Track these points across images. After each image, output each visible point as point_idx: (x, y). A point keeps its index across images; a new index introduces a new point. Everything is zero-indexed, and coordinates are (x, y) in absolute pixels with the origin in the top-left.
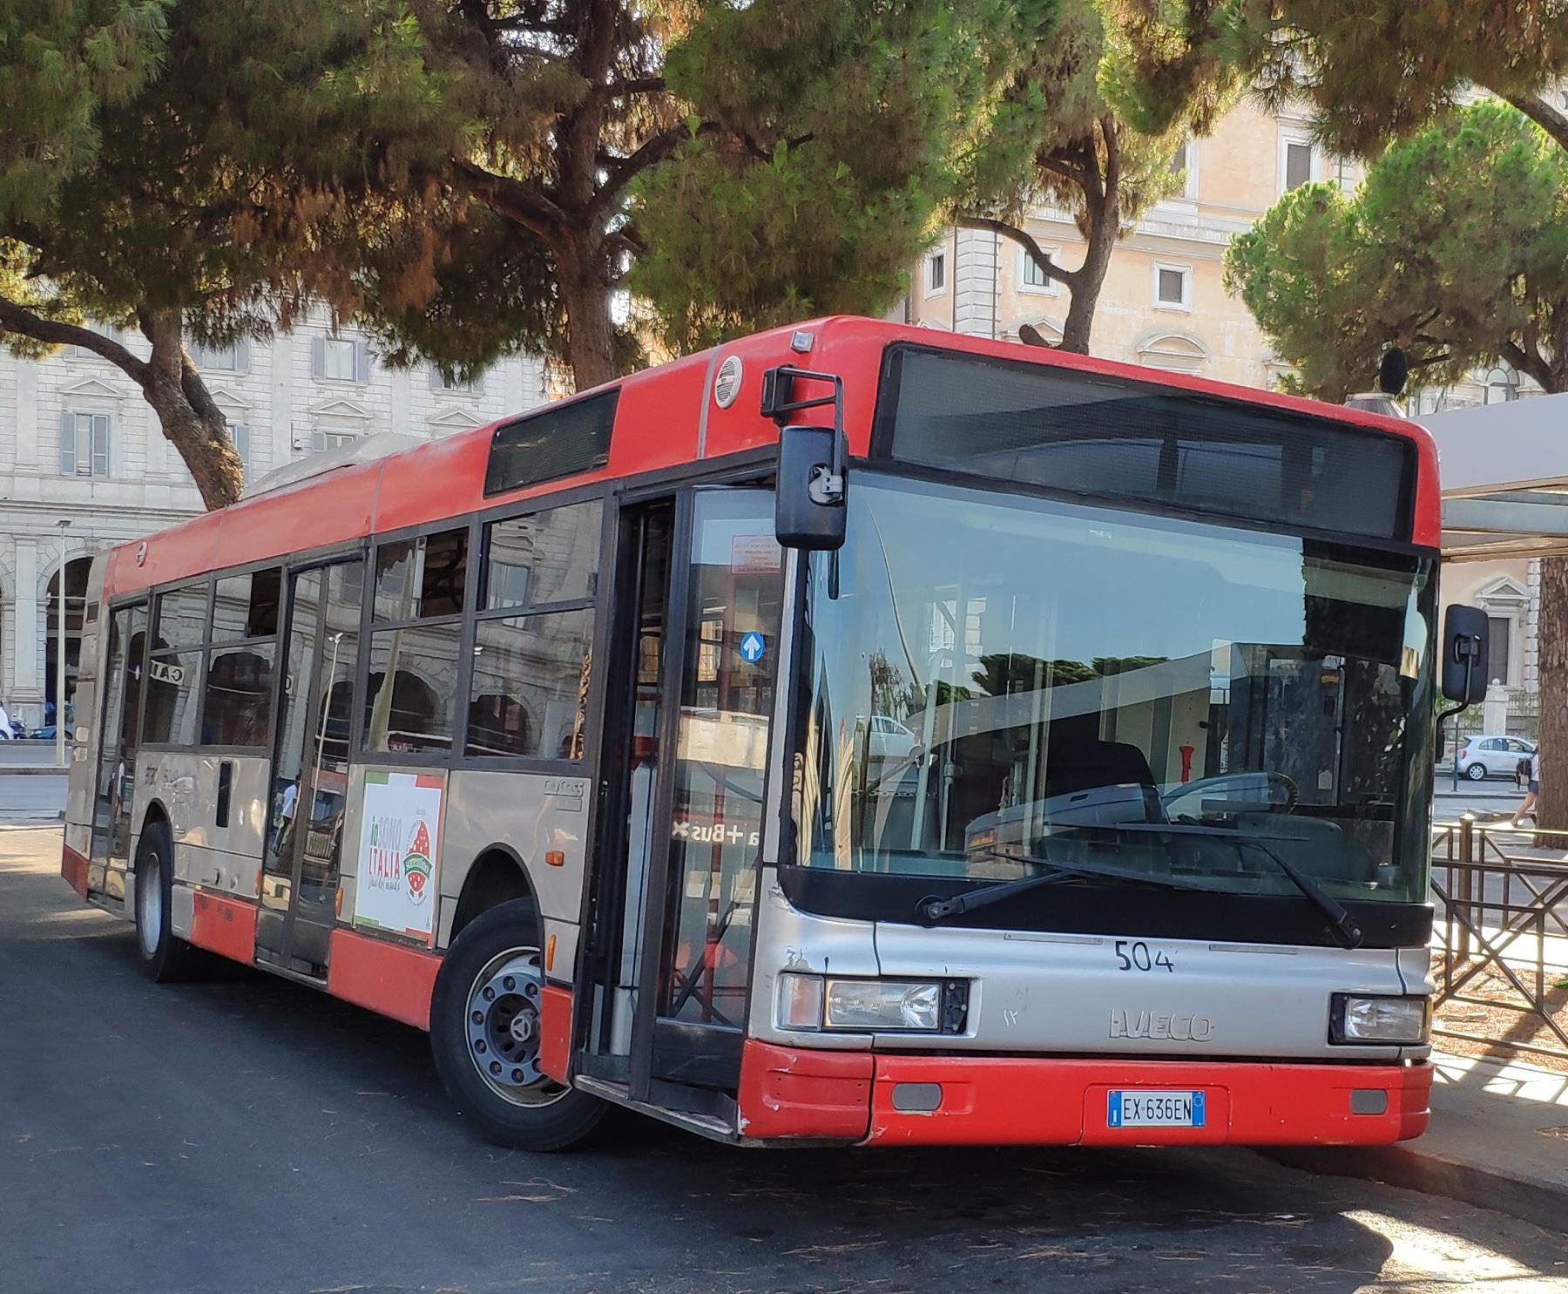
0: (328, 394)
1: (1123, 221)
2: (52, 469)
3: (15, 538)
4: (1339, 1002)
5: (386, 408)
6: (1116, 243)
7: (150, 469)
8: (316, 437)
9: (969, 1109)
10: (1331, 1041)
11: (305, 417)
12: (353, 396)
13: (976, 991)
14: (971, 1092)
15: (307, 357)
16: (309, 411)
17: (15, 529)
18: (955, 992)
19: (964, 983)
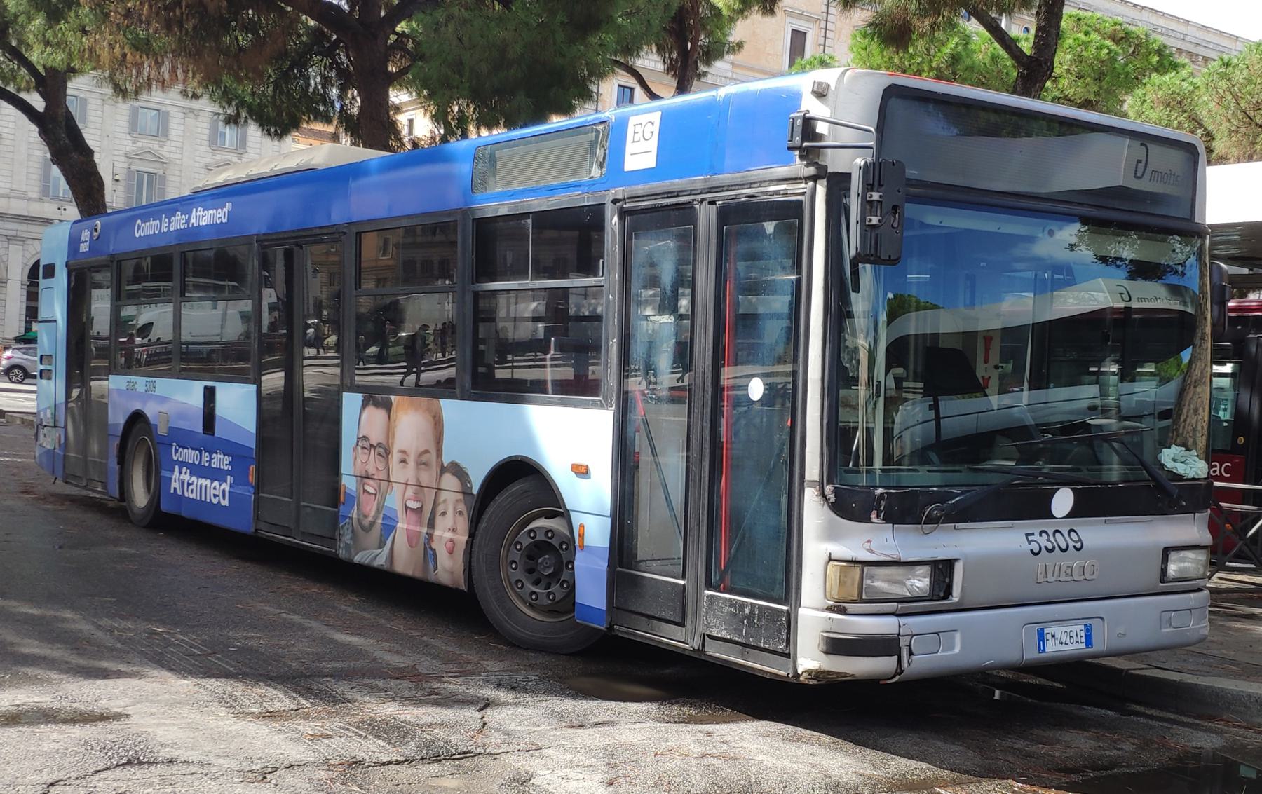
0: (139, 144)
1: (702, 68)
2: (35, 195)
3: (10, 239)
4: (1167, 551)
5: (179, 156)
6: (695, 82)
7: (14, 187)
8: (130, 173)
9: (957, 650)
10: (1162, 581)
11: (123, 159)
12: (156, 147)
13: (959, 568)
14: (958, 636)
15: (126, 118)
16: (126, 155)
17: (9, 233)
18: (942, 570)
19: (949, 564)
